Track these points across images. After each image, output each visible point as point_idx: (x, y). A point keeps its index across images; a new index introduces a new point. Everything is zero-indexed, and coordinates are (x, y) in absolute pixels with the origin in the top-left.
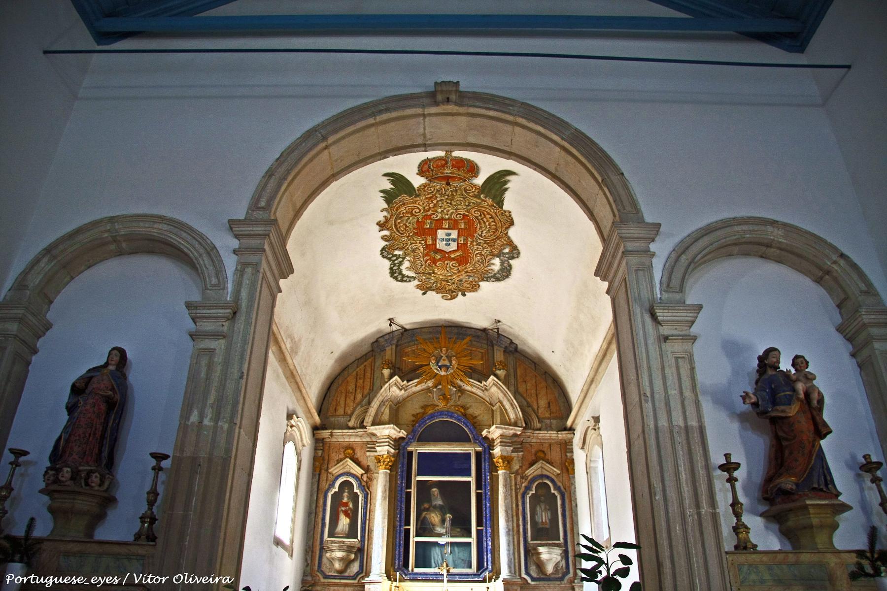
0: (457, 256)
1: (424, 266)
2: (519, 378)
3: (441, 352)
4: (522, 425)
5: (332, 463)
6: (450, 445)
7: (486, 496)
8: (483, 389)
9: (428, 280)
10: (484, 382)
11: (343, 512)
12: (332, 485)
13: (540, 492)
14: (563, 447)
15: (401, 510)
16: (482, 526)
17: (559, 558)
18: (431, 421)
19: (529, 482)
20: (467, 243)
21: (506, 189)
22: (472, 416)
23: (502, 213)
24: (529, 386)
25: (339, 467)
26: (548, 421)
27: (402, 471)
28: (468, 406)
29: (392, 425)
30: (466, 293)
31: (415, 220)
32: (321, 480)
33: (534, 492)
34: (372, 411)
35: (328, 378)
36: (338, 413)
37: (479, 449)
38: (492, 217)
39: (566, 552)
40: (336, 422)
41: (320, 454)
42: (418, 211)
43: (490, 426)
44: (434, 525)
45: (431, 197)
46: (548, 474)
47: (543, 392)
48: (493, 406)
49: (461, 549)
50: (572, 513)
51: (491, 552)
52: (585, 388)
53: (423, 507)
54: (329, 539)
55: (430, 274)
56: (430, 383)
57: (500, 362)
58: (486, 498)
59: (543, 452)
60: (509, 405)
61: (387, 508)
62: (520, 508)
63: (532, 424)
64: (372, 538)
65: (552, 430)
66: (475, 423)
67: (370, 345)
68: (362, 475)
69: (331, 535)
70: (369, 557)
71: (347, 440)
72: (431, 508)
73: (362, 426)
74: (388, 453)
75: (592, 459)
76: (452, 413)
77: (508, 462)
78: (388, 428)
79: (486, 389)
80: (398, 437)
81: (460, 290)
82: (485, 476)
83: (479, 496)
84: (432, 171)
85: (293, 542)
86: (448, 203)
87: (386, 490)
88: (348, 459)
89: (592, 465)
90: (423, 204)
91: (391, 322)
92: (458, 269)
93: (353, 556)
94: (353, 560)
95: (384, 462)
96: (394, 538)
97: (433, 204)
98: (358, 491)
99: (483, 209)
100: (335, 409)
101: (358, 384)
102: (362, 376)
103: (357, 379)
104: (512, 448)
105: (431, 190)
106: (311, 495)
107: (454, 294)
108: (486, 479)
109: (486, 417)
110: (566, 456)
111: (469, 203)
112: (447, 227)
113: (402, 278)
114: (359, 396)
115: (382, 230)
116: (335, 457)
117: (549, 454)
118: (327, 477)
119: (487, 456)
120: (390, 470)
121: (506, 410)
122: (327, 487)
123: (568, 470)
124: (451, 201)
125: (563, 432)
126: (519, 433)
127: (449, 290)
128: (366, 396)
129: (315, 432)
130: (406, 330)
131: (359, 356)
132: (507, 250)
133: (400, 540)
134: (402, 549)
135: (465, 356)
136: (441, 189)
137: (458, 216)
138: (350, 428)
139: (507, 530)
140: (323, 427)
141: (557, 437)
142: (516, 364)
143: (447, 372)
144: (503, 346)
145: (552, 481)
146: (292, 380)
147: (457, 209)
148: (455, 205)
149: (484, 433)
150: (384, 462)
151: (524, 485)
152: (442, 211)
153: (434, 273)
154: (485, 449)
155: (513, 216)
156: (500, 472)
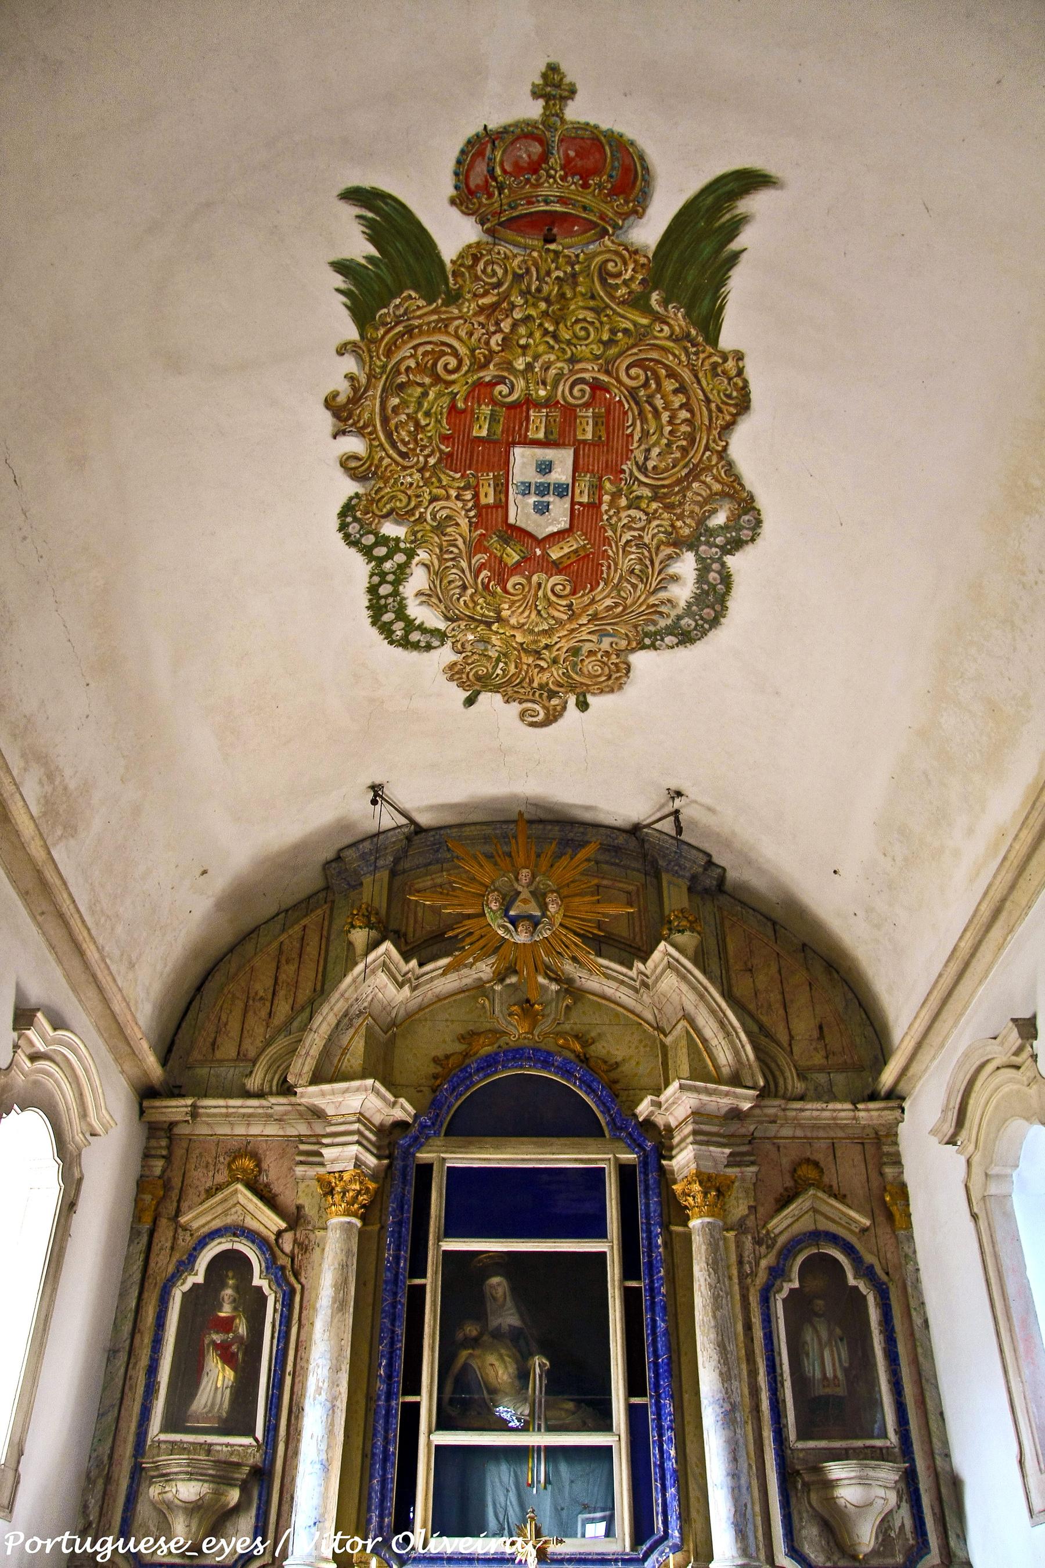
0: (567, 556)
1: (470, 591)
2: (731, 961)
3: (517, 880)
4: (756, 1083)
5: (192, 1196)
6: (542, 1146)
7: (653, 1298)
8: (637, 984)
9: (481, 646)
10: (638, 965)
11: (216, 1346)
12: (188, 1264)
13: (817, 1283)
14: (870, 1150)
15: (392, 1343)
16: (643, 1394)
17: (892, 1497)
18: (487, 1076)
19: (780, 1253)
20: (601, 503)
21: (734, 258)
22: (605, 1062)
23: (715, 366)
24: (762, 980)
25: (212, 1208)
26: (822, 1078)
27: (400, 1223)
28: (593, 1034)
29: (370, 1082)
30: (590, 699)
31: (445, 401)
32: (155, 1248)
33: (796, 1285)
34: (315, 1042)
35: (195, 953)
36: (218, 1055)
37: (629, 1157)
38: (682, 389)
39: (910, 1477)
40: (213, 1080)
41: (158, 1171)
42: (453, 363)
43: (658, 1091)
44: (493, 1391)
45: (494, 306)
46: (833, 1228)
47: (802, 999)
48: (666, 1035)
49: (578, 1468)
50: (915, 1347)
51: (677, 1480)
52: (966, 946)
53: (460, 1336)
54: (163, 1437)
55: (489, 625)
56: (485, 969)
57: (682, 911)
58: (653, 1303)
59: (816, 1164)
60: (715, 1026)
61: (348, 1337)
62: (758, 1334)
63: (781, 1081)
64: (299, 1433)
65: (834, 1098)
66: (616, 1082)
67: (318, 867)
68: (279, 1234)
69: (174, 1422)
70: (287, 1497)
71: (240, 1130)
72: (485, 1338)
73: (287, 1089)
74: (356, 1166)
75: (994, 1170)
76: (549, 1053)
77: (720, 1193)
78: (358, 1089)
79: (645, 984)
80: (390, 1120)
81: (572, 688)
82: (649, 1238)
83: (631, 1298)
84: (501, 190)
85: (21, 1453)
86: (546, 332)
87: (345, 1281)
88: (240, 1187)
89: (993, 1189)
90: (470, 334)
91: (376, 795)
92: (570, 606)
93: (234, 1496)
94: (236, 1510)
95: (344, 1192)
96: (370, 1433)
97: (498, 337)
98: (264, 1284)
99: (654, 355)
100: (213, 1044)
101: (282, 977)
102: (295, 955)
103: (279, 962)
104: (727, 1151)
105: (494, 273)
106: (122, 1295)
107: (555, 701)
108: (651, 1246)
109: (644, 1069)
110: (881, 1174)
111: (613, 332)
112: (541, 435)
113: (407, 631)
114: (283, 1009)
115: (344, 433)
116: (201, 1178)
117: (833, 1171)
118: (175, 1238)
119: (652, 1176)
120: (363, 1218)
121: (705, 1041)
122: (171, 1269)
123: (890, 1217)
124: (557, 324)
125: (872, 1105)
126: (746, 1106)
127: (541, 687)
128: (303, 1008)
129: (145, 1103)
130: (419, 830)
131: (289, 901)
132: (720, 519)
133: (387, 1441)
134: (393, 1473)
135: (581, 894)
136: (528, 271)
137: (576, 391)
138: (248, 1095)
139: (727, 1406)
140: (174, 1091)
141: (855, 1118)
142: (722, 923)
143: (532, 934)
144: (688, 874)
145: (849, 1249)
146: (45, 906)
147: (573, 360)
148: (569, 343)
149: (644, 1109)
150: (344, 1192)
151: (764, 1263)
152: (529, 367)
153: (499, 619)
154: (646, 1156)
155: (751, 372)
156: (695, 1223)
